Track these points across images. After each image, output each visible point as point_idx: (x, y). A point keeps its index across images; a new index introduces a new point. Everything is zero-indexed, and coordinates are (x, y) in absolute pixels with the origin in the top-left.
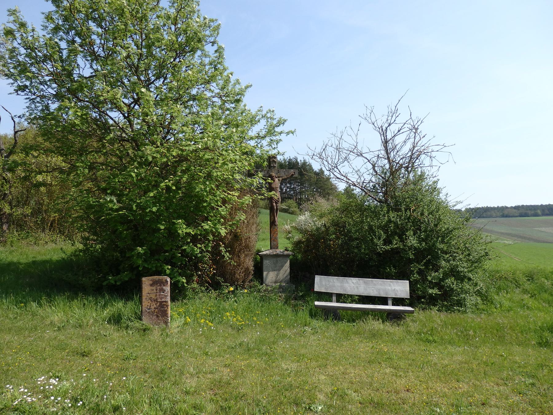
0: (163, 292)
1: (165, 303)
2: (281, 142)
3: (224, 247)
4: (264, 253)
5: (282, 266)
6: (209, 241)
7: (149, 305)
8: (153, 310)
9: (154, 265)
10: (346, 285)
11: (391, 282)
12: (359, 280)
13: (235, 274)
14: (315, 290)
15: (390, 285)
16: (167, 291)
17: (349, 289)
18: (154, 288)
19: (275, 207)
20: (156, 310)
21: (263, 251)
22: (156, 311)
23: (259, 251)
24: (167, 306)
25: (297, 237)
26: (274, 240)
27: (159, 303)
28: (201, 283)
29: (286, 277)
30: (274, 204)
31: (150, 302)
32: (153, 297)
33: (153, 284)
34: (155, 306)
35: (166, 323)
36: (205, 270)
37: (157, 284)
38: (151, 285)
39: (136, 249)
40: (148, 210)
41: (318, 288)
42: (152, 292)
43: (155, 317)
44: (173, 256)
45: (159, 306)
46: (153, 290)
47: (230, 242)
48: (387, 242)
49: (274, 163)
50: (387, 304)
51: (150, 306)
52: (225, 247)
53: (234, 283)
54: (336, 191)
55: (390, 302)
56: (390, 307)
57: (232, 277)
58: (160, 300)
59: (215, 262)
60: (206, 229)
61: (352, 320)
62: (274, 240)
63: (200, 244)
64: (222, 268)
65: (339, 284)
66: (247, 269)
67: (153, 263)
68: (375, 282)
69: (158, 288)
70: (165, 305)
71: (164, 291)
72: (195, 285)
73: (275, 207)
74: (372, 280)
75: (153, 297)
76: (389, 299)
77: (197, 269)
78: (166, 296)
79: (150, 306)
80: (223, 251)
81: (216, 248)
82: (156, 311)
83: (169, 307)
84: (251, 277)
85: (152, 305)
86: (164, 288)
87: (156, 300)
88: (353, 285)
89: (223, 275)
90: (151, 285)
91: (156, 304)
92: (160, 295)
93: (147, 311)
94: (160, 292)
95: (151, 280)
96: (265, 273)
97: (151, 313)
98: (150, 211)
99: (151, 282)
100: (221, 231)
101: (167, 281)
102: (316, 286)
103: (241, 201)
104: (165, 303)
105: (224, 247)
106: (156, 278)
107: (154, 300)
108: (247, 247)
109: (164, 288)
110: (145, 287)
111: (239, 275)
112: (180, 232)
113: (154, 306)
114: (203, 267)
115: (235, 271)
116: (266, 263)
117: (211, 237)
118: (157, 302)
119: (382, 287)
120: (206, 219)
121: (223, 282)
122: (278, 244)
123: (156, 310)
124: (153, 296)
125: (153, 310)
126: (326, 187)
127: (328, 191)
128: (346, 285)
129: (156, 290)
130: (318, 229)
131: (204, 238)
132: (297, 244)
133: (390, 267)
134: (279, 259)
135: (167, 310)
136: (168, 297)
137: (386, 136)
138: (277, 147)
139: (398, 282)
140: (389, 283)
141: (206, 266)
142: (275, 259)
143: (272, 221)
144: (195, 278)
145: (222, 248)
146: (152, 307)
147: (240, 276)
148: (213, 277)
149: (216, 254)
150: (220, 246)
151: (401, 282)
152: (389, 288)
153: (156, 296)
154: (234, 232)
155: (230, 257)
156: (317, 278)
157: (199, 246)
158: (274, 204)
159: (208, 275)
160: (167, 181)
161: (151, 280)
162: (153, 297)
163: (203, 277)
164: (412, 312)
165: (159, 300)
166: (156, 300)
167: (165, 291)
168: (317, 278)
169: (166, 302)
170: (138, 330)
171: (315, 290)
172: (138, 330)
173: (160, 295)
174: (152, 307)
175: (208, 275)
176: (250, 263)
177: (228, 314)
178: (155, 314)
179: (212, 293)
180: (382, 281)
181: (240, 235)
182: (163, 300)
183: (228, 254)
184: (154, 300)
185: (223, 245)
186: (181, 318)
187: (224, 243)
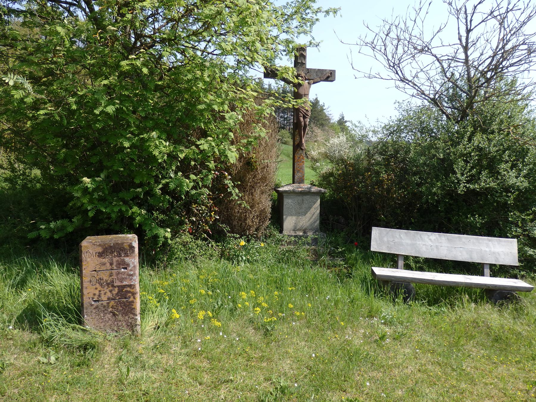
0: (126, 268)
1: (128, 289)
2: (317, 23)
3: (230, 179)
4: (286, 189)
5: (310, 208)
6: (210, 170)
7: (97, 292)
8: (105, 303)
9: (116, 209)
10: (419, 243)
11: (490, 241)
12: (440, 236)
13: (245, 219)
14: (372, 249)
15: (488, 246)
16: (132, 265)
17: (424, 249)
18: (106, 260)
19: (303, 123)
20: (112, 303)
21: (282, 186)
22: (111, 304)
23: (277, 186)
24: (134, 294)
25: (326, 167)
26: (299, 171)
27: (116, 289)
28: (195, 234)
29: (315, 222)
30: (302, 119)
31: (99, 288)
32: (105, 278)
33: (103, 252)
34: (109, 295)
35: (132, 327)
36: (202, 214)
37: (112, 253)
38: (100, 255)
39: (82, 182)
40: (97, 112)
41: (376, 247)
42: (103, 268)
43: (109, 316)
44: (149, 193)
45: (117, 294)
46: (104, 264)
47: (239, 172)
48: (472, 179)
49: (302, 58)
50: (482, 275)
51: (99, 296)
52: (233, 180)
53: (244, 231)
54: (329, 122)
55: (487, 271)
56: (487, 280)
57: (241, 224)
58: (119, 284)
59: (217, 201)
60: (204, 150)
61: (433, 301)
62: (299, 171)
63: (194, 174)
64: (227, 210)
65: (409, 242)
66: (263, 211)
67: (115, 205)
68: (464, 240)
69: (115, 259)
70: (130, 292)
71: (126, 266)
72: (187, 238)
73: (303, 123)
74: (459, 237)
75: (105, 278)
76: (485, 265)
77: (190, 212)
78: (132, 275)
79: (99, 296)
80: (230, 185)
81: (219, 180)
82: (111, 304)
83: (138, 296)
84: (268, 223)
85: (102, 292)
86: (127, 259)
87: (111, 284)
88: (430, 243)
89: (228, 220)
90: (100, 255)
91: (111, 291)
92: (118, 274)
93: (92, 305)
94: (119, 268)
95: (100, 245)
96: (284, 217)
97: (101, 309)
98: (102, 112)
99: (100, 250)
100: (229, 154)
101: (132, 248)
102: (373, 243)
103: (260, 107)
104: (128, 289)
105: (230, 179)
106: (112, 239)
107: (108, 284)
108: (264, 179)
109: (127, 259)
110: (88, 260)
111: (252, 221)
112: (156, 153)
113: (106, 294)
114: (199, 210)
115: (246, 216)
116: (288, 202)
117: (212, 165)
118: (113, 286)
119: (476, 248)
120: (204, 134)
121: (228, 232)
122: (303, 176)
123: (112, 303)
124: (105, 277)
125: (105, 303)
126: (320, 117)
127: (323, 122)
128: (419, 243)
129: (111, 264)
130: (358, 158)
131: (200, 165)
132: (326, 179)
133: (473, 215)
134: (305, 197)
135: (133, 302)
136: (135, 278)
137: (471, 21)
138: (311, 32)
139: (500, 241)
140: (487, 242)
141: (204, 207)
142: (300, 198)
143: (296, 143)
144: (187, 227)
145: (228, 182)
146: (104, 298)
147: (253, 222)
148: (213, 226)
149: (219, 190)
150: (225, 177)
151: (505, 241)
152: (487, 249)
153: (111, 275)
154: (246, 158)
155: (240, 195)
156: (376, 232)
157: (193, 177)
158: (302, 119)
159: (207, 223)
160: (134, 56)
161: (100, 245)
162: (105, 278)
163: (199, 224)
164: (528, 290)
165: (117, 283)
166: (111, 284)
167: (128, 265)
168: (376, 232)
169: (130, 286)
170: (70, 349)
171: (372, 249)
172: (70, 349)
173: (118, 274)
174: (104, 298)
175: (207, 223)
176: (266, 204)
177: (244, 295)
178: (110, 309)
179: (212, 246)
180: (475, 238)
181: (256, 162)
182: (125, 283)
183: (237, 191)
184: (108, 284)
185: (230, 177)
186: (162, 306)
187: (230, 174)
